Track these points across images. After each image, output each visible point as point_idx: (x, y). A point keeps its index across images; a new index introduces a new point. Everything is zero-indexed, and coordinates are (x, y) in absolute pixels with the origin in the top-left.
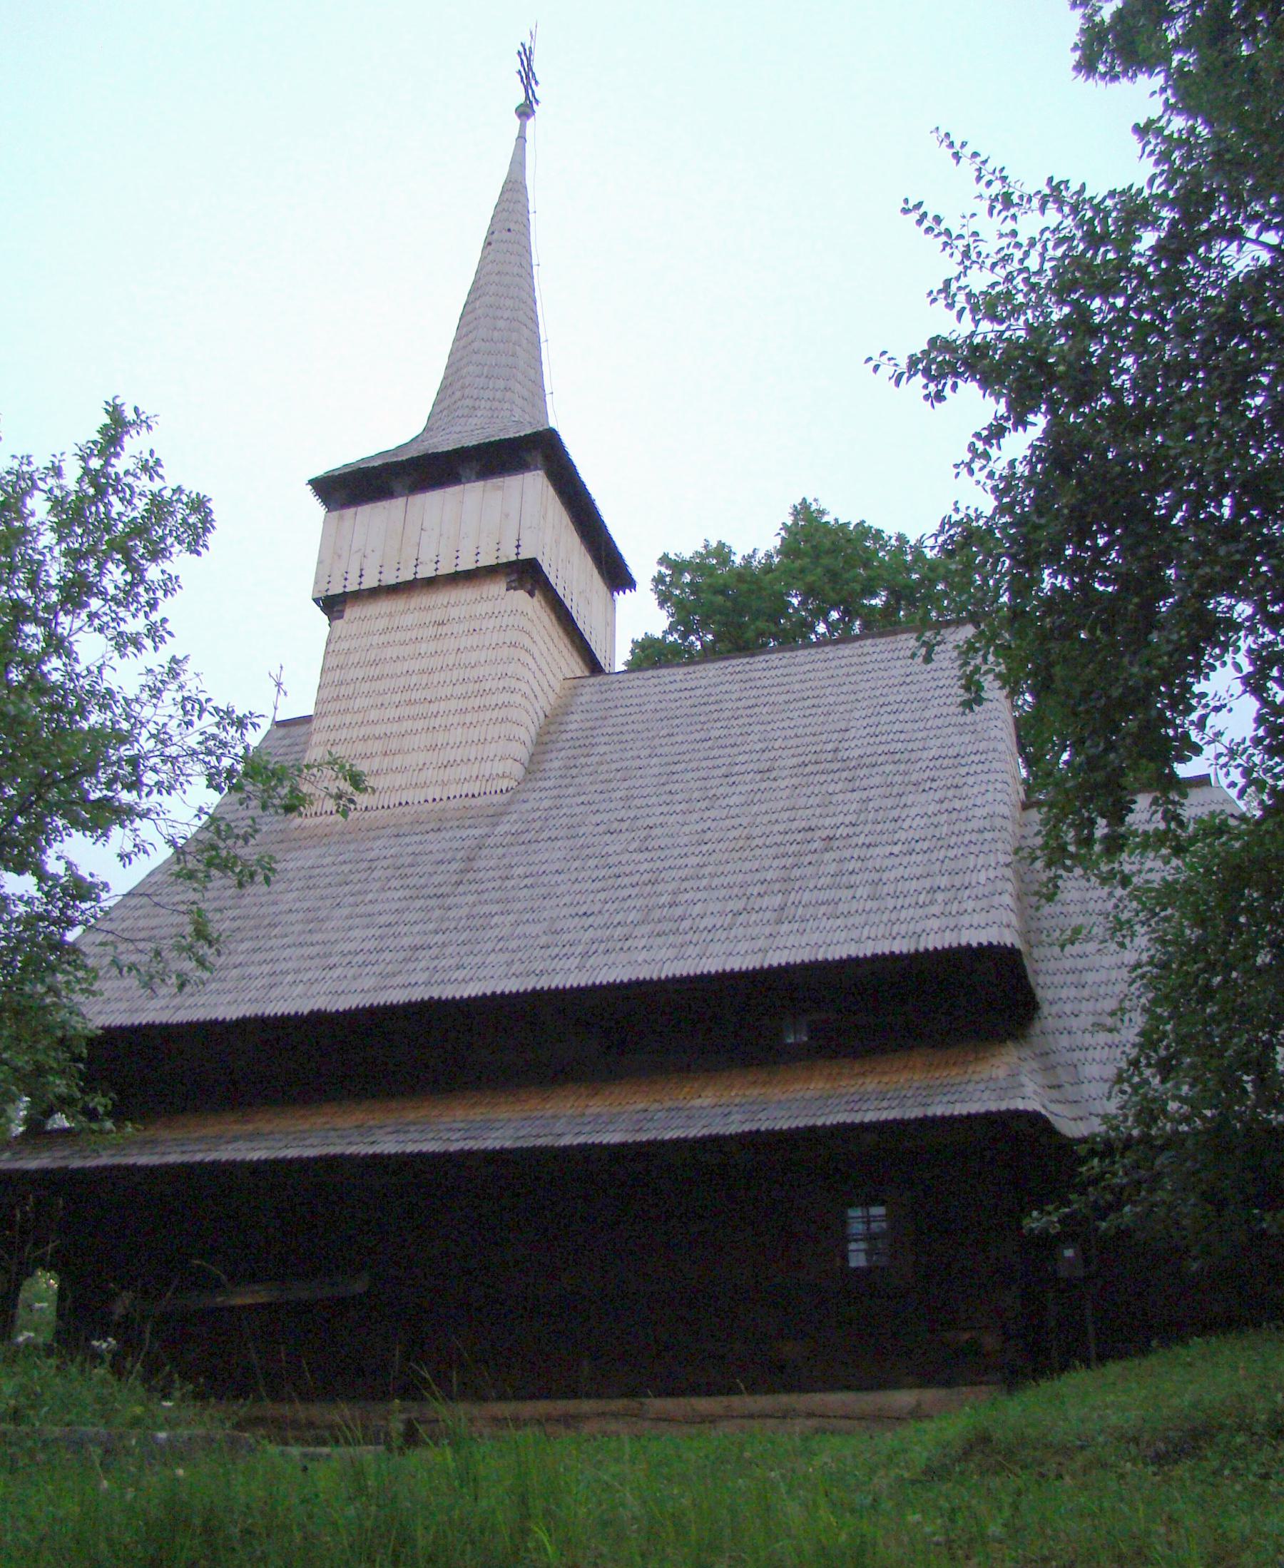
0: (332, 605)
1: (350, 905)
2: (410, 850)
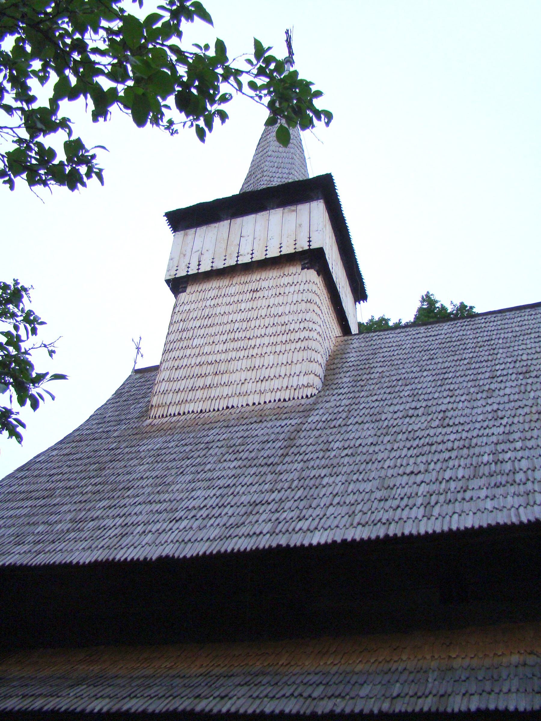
0: (177, 285)
1: (192, 473)
2: (239, 434)
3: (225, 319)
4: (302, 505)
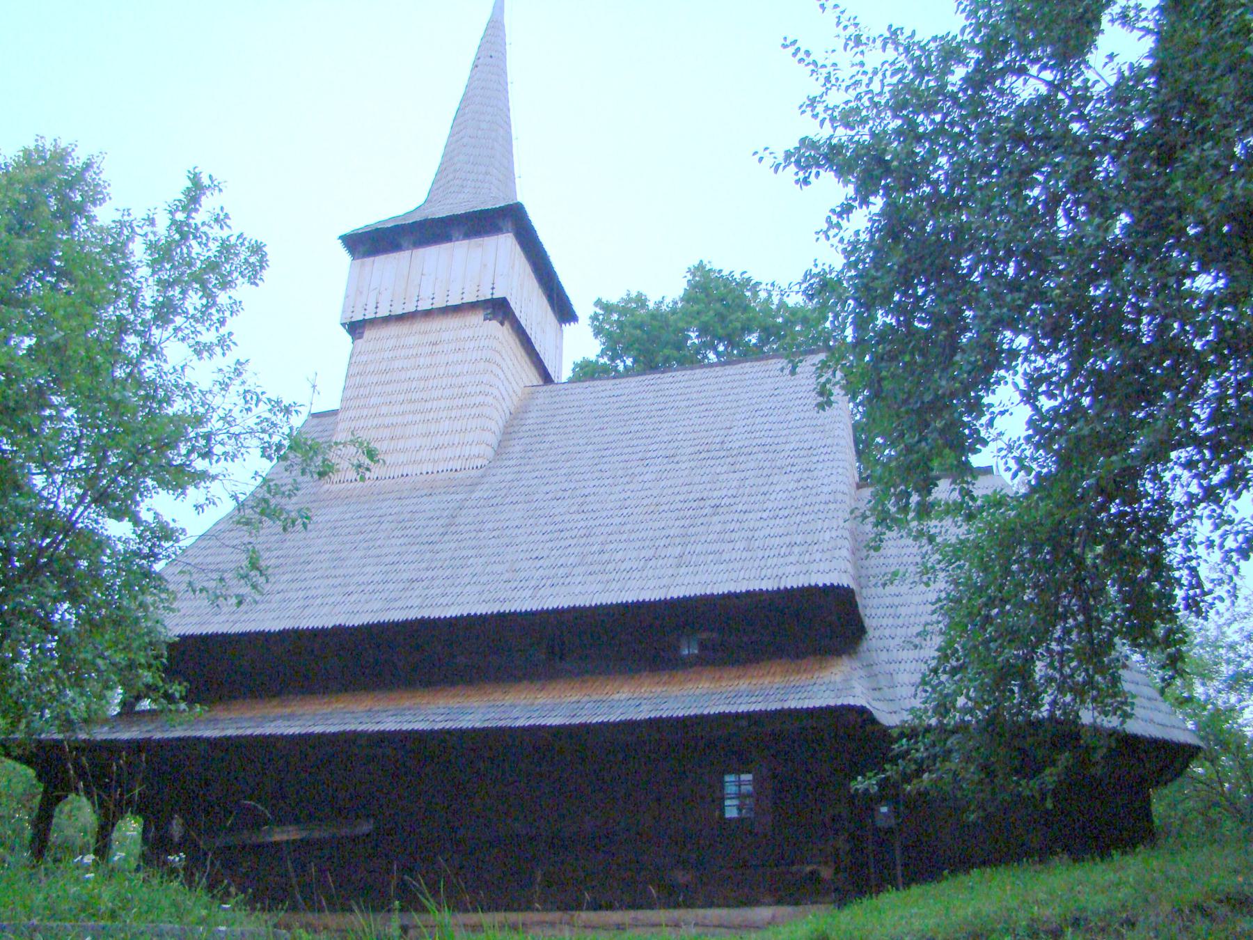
0: (355, 328)
4: (449, 582)
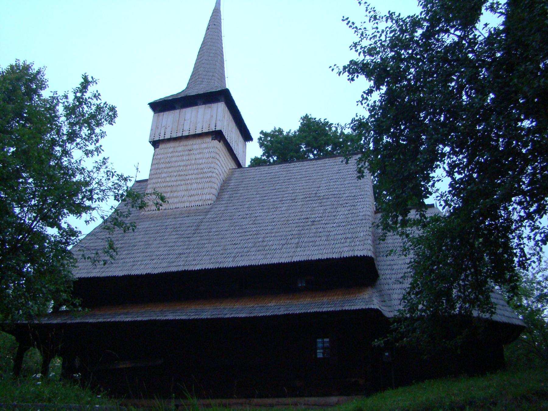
0: (155, 144)
3: (176, 164)
